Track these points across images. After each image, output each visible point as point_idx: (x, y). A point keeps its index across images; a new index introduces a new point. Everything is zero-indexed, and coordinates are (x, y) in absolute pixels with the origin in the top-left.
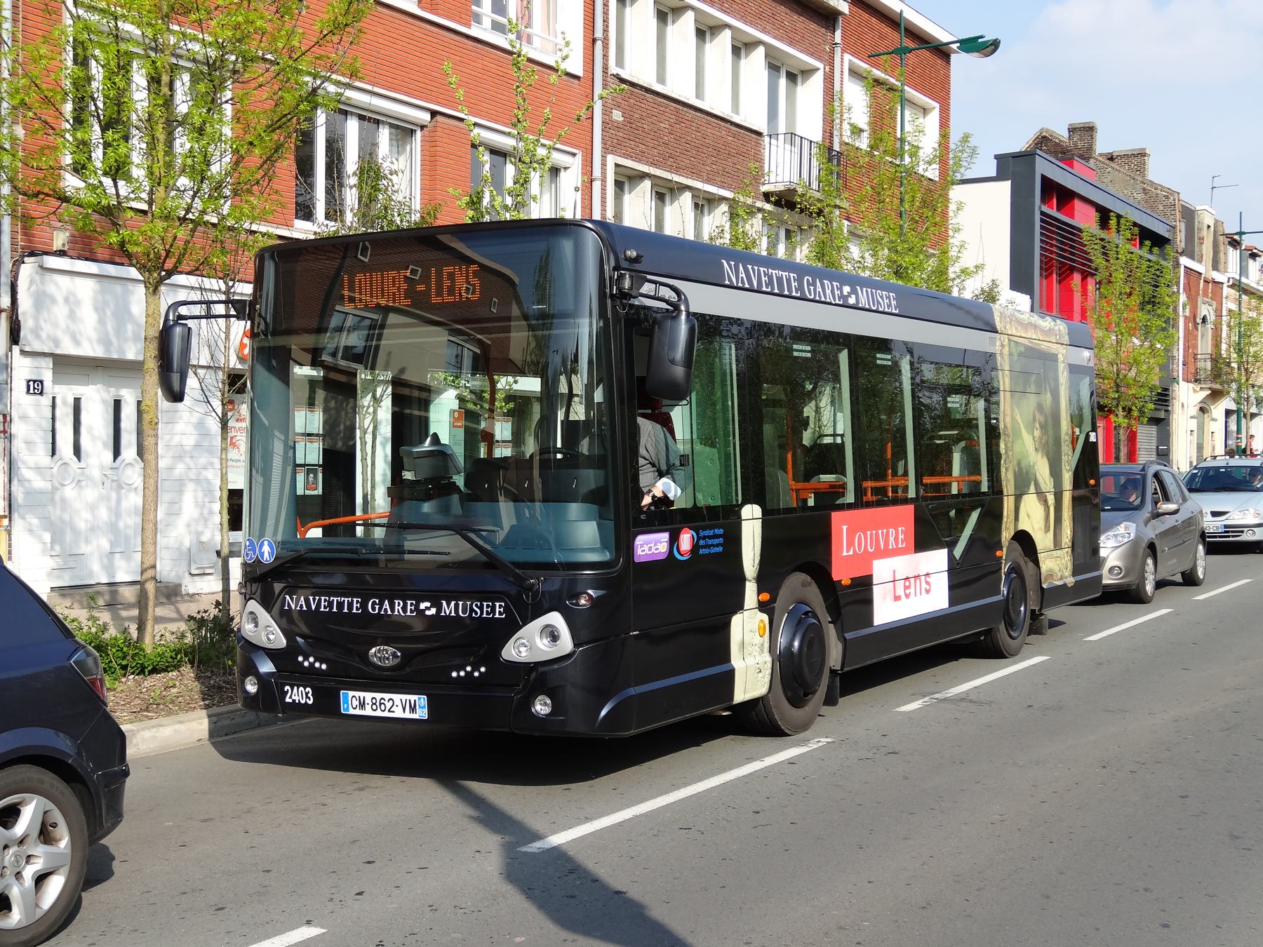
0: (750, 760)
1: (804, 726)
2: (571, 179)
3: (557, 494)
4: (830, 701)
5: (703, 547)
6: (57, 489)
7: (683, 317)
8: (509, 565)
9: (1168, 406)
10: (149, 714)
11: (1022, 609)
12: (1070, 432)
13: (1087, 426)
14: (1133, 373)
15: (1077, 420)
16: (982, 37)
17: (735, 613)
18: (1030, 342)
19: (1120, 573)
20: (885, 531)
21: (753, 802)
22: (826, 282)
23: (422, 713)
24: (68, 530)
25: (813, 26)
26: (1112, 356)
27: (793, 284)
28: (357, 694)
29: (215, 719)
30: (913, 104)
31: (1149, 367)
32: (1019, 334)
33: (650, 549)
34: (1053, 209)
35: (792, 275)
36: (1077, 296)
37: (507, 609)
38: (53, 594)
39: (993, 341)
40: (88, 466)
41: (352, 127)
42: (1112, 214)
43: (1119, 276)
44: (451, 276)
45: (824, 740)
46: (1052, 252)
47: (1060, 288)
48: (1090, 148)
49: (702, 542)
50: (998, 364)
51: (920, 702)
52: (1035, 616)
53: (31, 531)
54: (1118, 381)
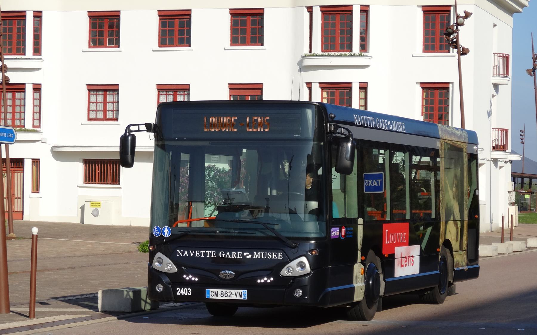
18: (453, 143)
22: (383, 120)
28: (214, 290)
32: (448, 139)
35: (373, 118)
44: (256, 121)
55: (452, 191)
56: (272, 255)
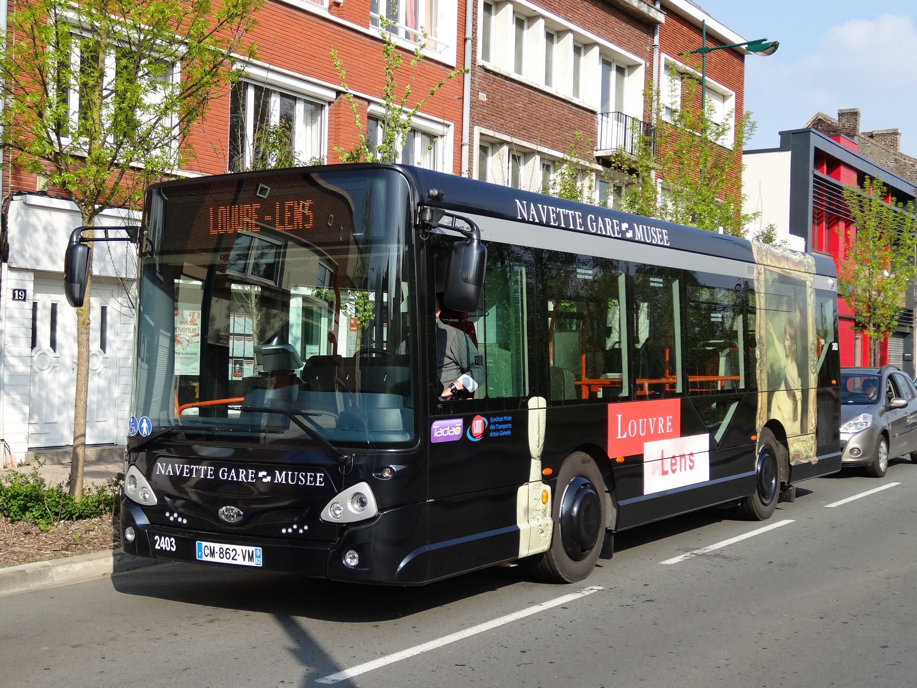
0: (531, 604)
1: (583, 575)
2: (445, 146)
3: (372, 387)
4: (606, 554)
5: (493, 431)
6: (37, 373)
7: (475, 244)
8: (330, 445)
9: (912, 323)
10: (66, 552)
11: (774, 482)
12: (816, 342)
13: (831, 338)
14: (881, 299)
15: (822, 334)
16: (765, 40)
17: (522, 484)
19: (859, 454)
20: (655, 419)
21: (524, 642)
22: (607, 219)
23: (258, 562)
24: (45, 404)
25: (637, 32)
26: (865, 285)
27: (578, 221)
28: (209, 544)
29: (119, 557)
30: (714, 92)
31: (894, 293)
32: (773, 265)
33: (445, 432)
34: (823, 173)
35: (577, 213)
36: (842, 239)
37: (325, 479)
38: (30, 453)
39: (751, 270)
40: (61, 355)
41: (275, 103)
42: (867, 176)
43: (872, 223)
44: (291, 209)
45: (596, 588)
46: (822, 206)
47: (829, 233)
48: (855, 128)
49: (492, 427)
50: (755, 288)
51: (682, 557)
52: (784, 487)
53: (14, 404)
54: (870, 303)
55: (782, 346)
56: (306, 479)
